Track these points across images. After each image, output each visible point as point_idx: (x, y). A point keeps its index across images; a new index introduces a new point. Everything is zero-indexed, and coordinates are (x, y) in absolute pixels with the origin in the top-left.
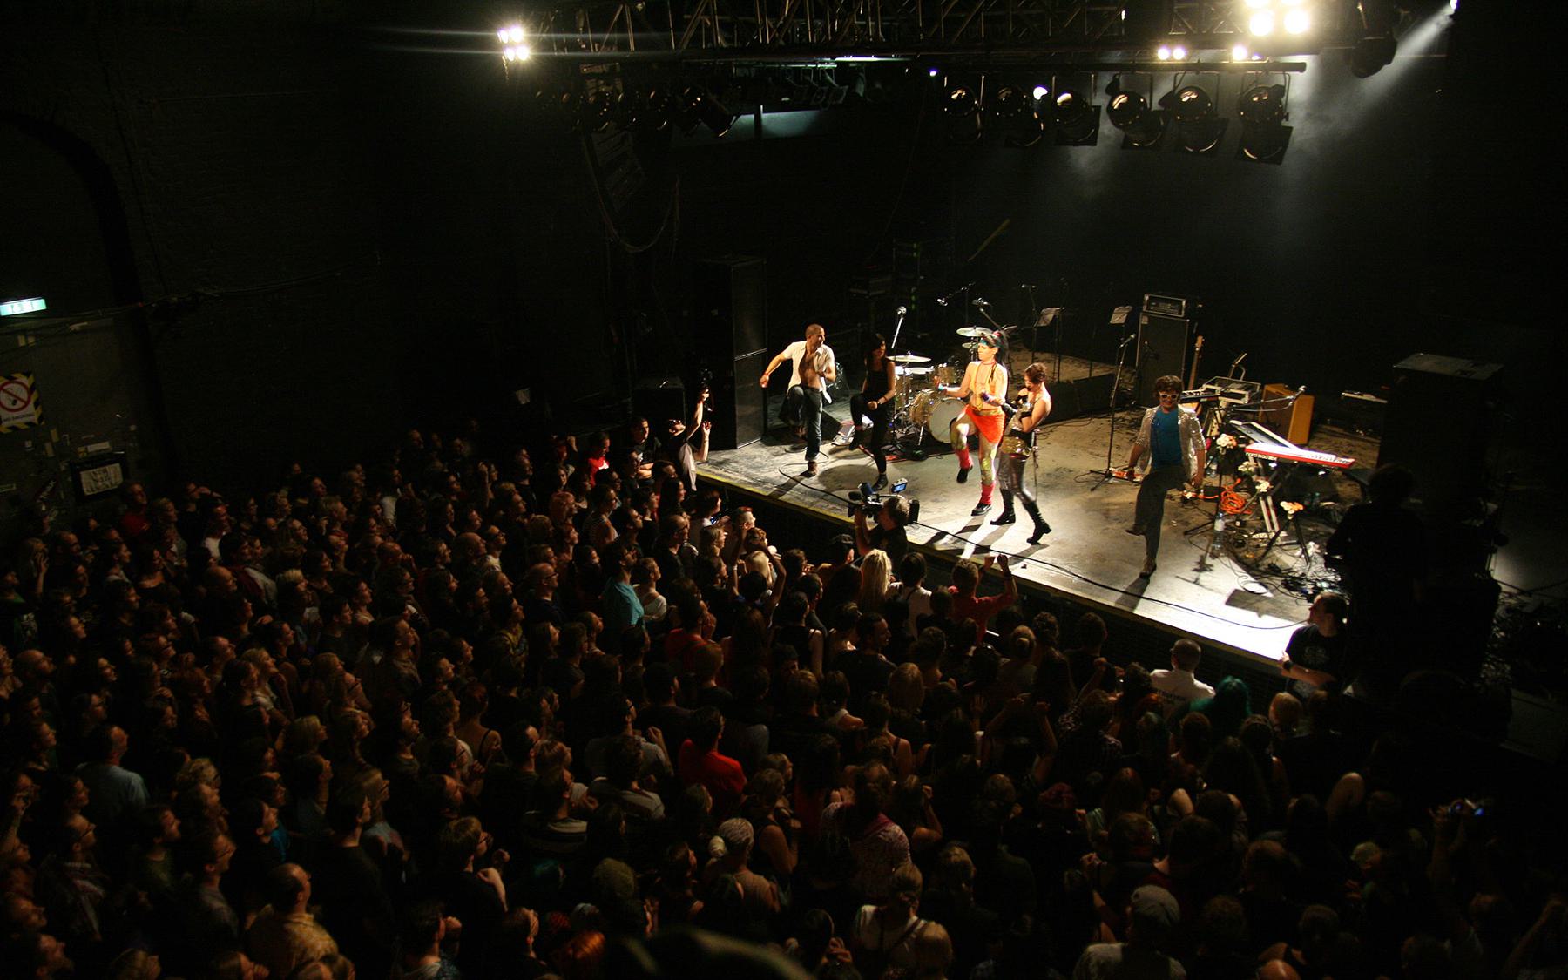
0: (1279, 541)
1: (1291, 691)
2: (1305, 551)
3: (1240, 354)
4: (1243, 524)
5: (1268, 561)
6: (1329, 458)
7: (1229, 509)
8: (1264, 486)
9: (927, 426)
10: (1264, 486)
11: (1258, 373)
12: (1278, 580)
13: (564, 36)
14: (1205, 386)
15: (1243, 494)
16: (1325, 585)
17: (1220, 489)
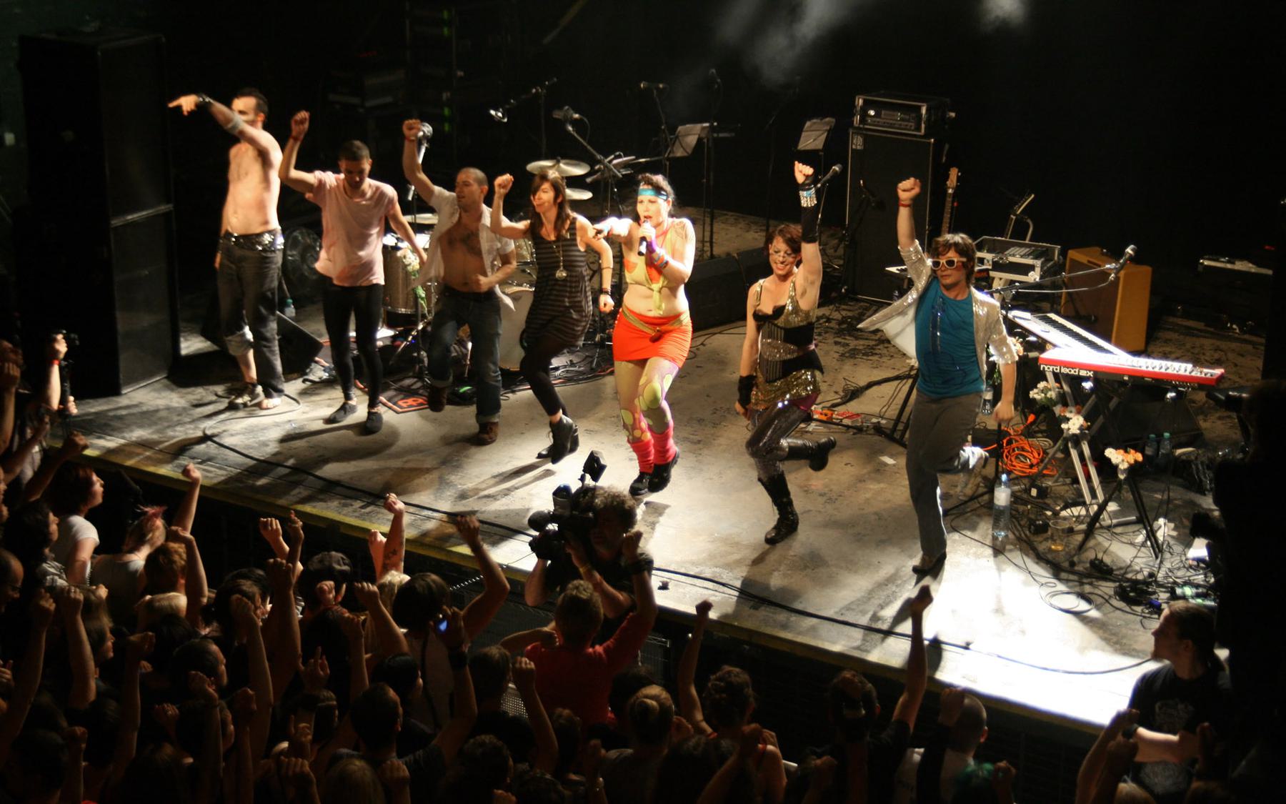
0: (1106, 520)
1: (1136, 780)
2: (1151, 535)
3: (1022, 197)
4: (1043, 493)
5: (1090, 555)
6: (1181, 368)
7: (1019, 467)
8: (1075, 423)
10: (1075, 423)
11: (1058, 228)
12: (1108, 588)
15: (1043, 442)
16: (1188, 591)
17: (603, 346)
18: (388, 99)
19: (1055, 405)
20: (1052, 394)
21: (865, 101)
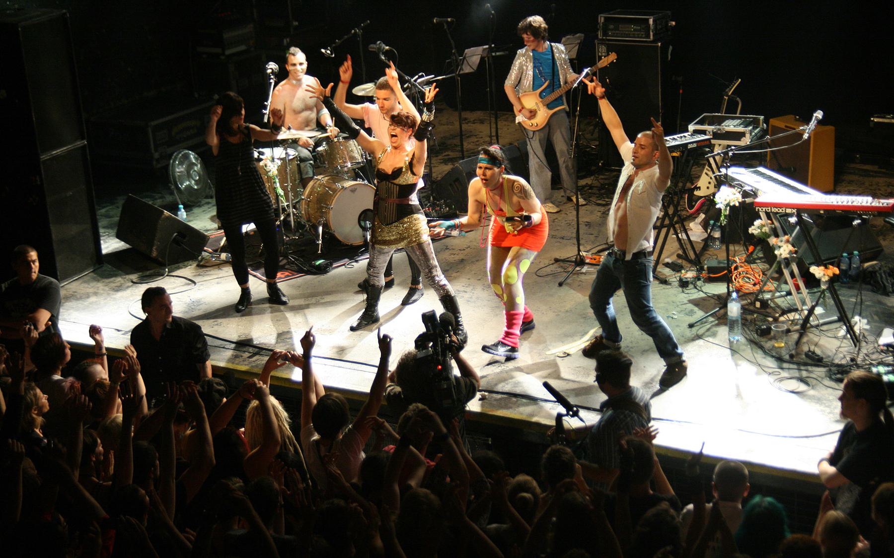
0: (813, 321)
2: (850, 329)
9: (326, 226)
11: (752, 104)
13: (616, 197)
14: (691, 127)
18: (243, 48)
19: (769, 236)
20: (766, 229)
21: (605, 18)
